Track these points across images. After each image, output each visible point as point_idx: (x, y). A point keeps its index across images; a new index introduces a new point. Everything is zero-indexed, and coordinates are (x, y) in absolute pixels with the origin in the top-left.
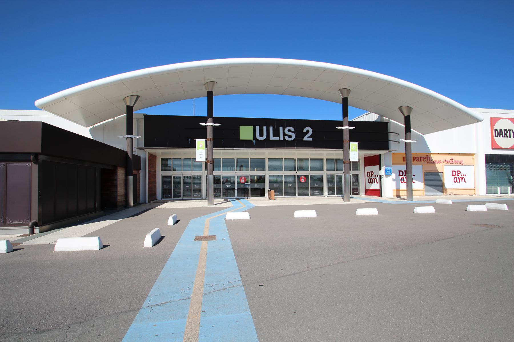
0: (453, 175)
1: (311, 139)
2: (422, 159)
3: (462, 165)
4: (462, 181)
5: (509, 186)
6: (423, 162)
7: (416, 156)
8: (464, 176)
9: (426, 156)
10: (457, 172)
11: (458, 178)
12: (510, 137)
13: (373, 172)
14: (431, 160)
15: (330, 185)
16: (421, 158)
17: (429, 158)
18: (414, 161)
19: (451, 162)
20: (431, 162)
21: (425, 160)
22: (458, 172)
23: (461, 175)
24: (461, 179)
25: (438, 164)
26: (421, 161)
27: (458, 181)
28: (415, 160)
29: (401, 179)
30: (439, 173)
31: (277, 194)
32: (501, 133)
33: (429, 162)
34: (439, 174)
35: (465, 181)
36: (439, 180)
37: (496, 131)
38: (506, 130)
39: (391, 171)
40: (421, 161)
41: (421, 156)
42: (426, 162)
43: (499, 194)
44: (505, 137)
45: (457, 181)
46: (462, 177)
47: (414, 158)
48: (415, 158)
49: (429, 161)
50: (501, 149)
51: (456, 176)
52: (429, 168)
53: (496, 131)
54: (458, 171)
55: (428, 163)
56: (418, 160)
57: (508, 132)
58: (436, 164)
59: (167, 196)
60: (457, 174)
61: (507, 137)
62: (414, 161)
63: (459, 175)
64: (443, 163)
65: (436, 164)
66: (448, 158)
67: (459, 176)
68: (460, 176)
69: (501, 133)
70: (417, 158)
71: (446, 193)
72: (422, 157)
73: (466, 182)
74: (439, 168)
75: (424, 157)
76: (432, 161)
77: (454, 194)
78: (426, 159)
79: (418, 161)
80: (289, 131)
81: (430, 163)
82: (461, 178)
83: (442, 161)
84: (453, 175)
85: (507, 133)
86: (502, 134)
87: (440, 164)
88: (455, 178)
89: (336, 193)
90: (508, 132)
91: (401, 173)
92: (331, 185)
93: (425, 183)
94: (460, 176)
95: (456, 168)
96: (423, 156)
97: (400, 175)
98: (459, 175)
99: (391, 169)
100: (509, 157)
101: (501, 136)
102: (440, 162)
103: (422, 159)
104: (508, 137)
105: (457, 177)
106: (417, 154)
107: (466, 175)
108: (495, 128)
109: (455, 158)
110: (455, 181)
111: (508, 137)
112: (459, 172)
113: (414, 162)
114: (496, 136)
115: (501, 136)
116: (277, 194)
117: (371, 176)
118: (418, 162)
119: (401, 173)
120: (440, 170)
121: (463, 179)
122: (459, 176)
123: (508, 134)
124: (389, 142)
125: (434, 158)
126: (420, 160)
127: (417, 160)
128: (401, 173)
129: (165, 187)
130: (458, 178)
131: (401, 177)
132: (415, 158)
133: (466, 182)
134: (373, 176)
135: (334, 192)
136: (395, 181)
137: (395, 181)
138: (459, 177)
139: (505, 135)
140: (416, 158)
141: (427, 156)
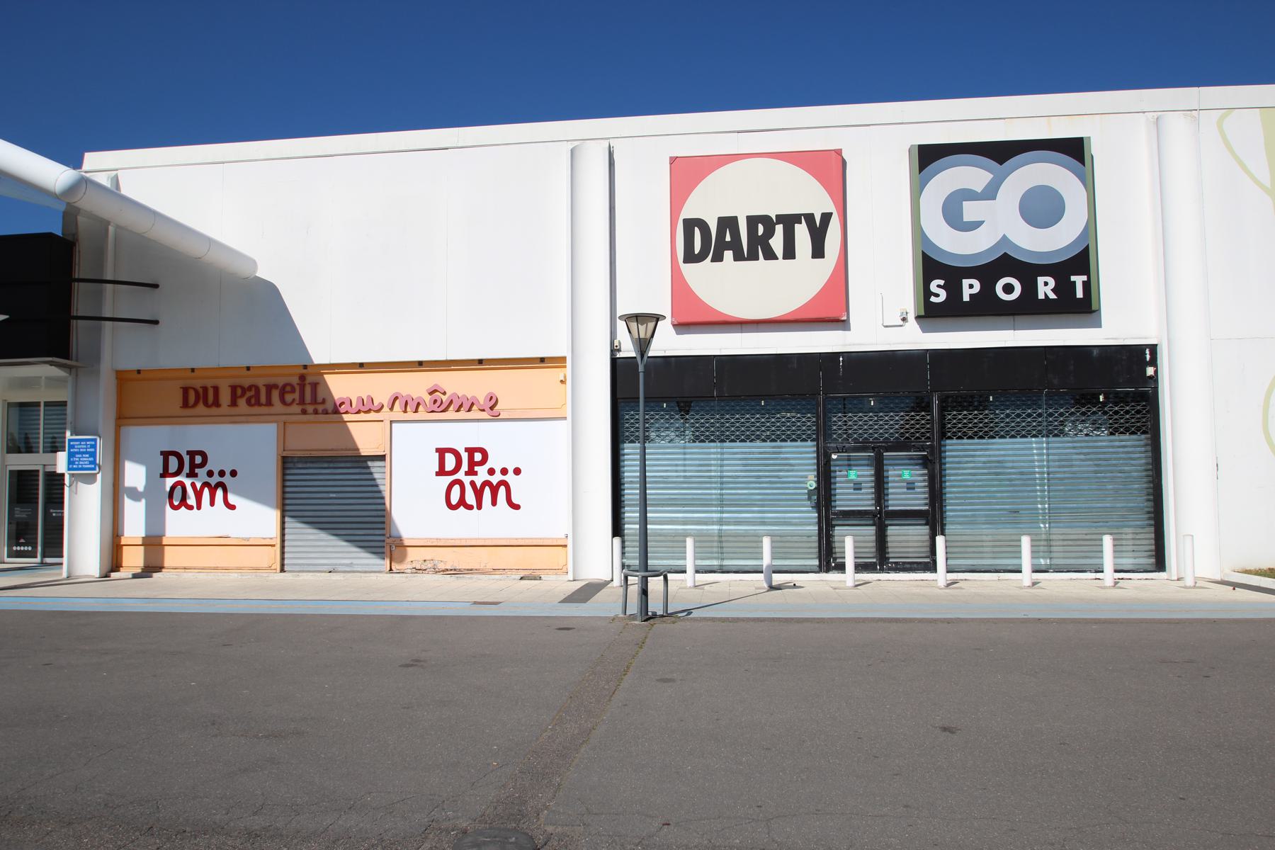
0: (442, 472)
1: (1041, 296)
2: (275, 395)
3: (496, 418)
4: (212, 504)
5: (1105, 522)
6: (278, 406)
7: (246, 383)
8: (510, 478)
9: (295, 381)
10: (187, 459)
11: (473, 483)
12: (790, 253)
13: (204, 455)
14: (320, 399)
15: (21, 513)
16: (270, 388)
17: (315, 386)
18: (234, 403)
19: (442, 405)
20: (320, 408)
21: (289, 398)
22: (471, 458)
23: (491, 472)
24: (487, 491)
25: (362, 416)
26: (269, 403)
27: (470, 498)
28: (242, 402)
29: (173, 488)
30: (370, 464)
31: (26, 548)
32: (728, 238)
33: (310, 409)
34: (368, 467)
35: (515, 500)
36: (370, 489)
37: (697, 232)
38: (765, 220)
39: (93, 455)
40: (269, 403)
41: (272, 381)
42: (296, 408)
43: (1108, 575)
44: (753, 256)
45: (462, 502)
46: (495, 479)
47: (234, 388)
48: (239, 392)
49: (314, 401)
50: (772, 325)
51: (460, 475)
52: (311, 438)
53: (697, 232)
54: (471, 451)
55: (304, 412)
56: (254, 401)
57: (779, 229)
58: (346, 417)
59: (22, 548)
60: (465, 467)
61: (770, 255)
62: (234, 403)
63: (476, 468)
64: (386, 409)
65: (346, 417)
66: (416, 385)
67: (475, 473)
68: (482, 475)
69: (728, 238)
70: (250, 388)
71: (402, 559)
72: (275, 386)
73: (516, 507)
74: (366, 437)
75: (285, 385)
76: (324, 401)
77: (442, 566)
78: (296, 395)
79: (258, 404)
80: (937, 295)
81: (316, 412)
82: (486, 483)
83: (382, 398)
84: (442, 472)
85: (770, 232)
86: (735, 246)
87: (372, 416)
88: (456, 489)
89: (39, 549)
90: (779, 229)
91: (173, 462)
92: (24, 516)
93: (380, 501)
94: (482, 475)
95: (461, 435)
96: (281, 382)
97: (165, 474)
98: (476, 468)
99: (94, 446)
100: (1095, 352)
101: (728, 254)
102: (367, 407)
103: (275, 395)
104: (776, 258)
105: (467, 480)
106: (139, 376)
107: (234, 473)
108: (689, 212)
109: (454, 383)
110: (454, 500)
111: (776, 258)
112: (477, 456)
113: (234, 410)
114: (690, 257)
115: (728, 254)
116: (26, 548)
117: (471, 472)
118: (256, 410)
119: (173, 462)
120: (365, 450)
121: (502, 490)
122: (475, 473)
123: (777, 243)
124: (74, 322)
125: (339, 387)
126: (263, 399)
127: (249, 402)
128: (173, 464)
129: (16, 516)
130: (473, 484)
131: (170, 482)
132: (239, 392)
133: (516, 507)
134: (202, 472)
135: (35, 547)
136: (144, 501)
137: (144, 501)
138: (479, 481)
139: (758, 248)
140: (244, 390)
141: (302, 378)
